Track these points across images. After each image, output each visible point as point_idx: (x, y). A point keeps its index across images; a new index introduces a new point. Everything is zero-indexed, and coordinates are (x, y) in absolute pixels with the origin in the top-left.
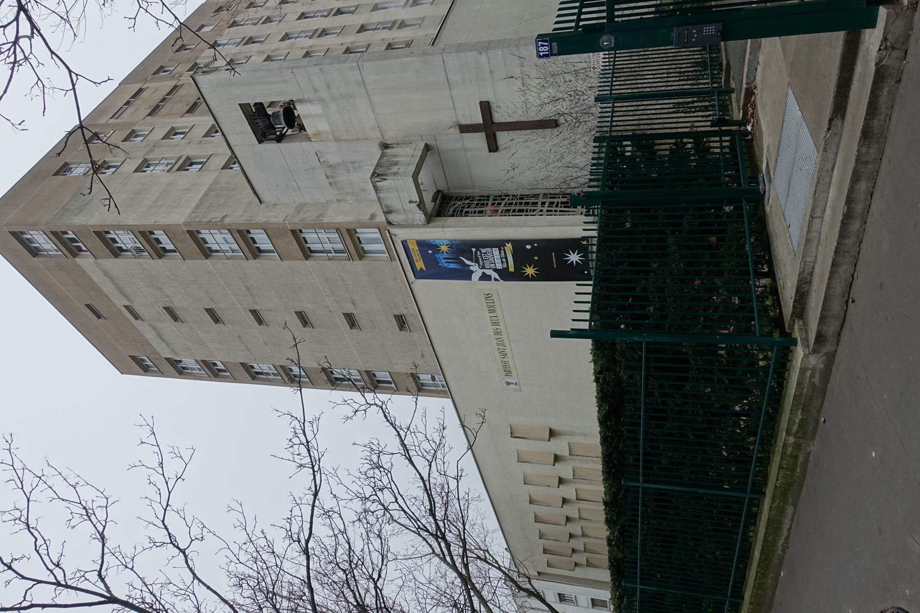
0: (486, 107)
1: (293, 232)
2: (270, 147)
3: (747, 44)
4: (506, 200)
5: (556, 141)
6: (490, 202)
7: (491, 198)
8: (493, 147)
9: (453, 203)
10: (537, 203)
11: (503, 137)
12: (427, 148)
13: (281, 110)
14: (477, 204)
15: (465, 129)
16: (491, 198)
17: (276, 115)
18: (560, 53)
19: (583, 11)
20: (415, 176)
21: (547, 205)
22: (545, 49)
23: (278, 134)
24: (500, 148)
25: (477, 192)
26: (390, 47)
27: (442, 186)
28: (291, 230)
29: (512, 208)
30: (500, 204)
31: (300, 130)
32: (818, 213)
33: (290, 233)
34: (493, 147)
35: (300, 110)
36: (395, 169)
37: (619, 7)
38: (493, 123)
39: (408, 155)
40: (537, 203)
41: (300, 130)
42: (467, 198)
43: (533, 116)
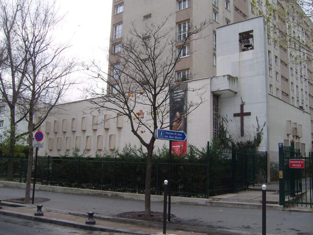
0: (249, 114)
1: (189, 19)
2: (237, 38)
3: (268, 206)
4: (217, 118)
5: (237, 136)
6: (216, 113)
7: (217, 113)
8: (236, 115)
9: (216, 99)
10: (216, 128)
11: (238, 118)
12: (236, 93)
13: (250, 44)
14: (216, 108)
15: (242, 106)
16: (217, 113)
17: (249, 42)
18: (279, 148)
19: (128, 113)
20: (229, 90)
21: (215, 132)
22: (280, 145)
23: (242, 40)
24: (235, 118)
25: (219, 108)
26: (271, 86)
27: (222, 96)
28: (190, 19)
29: (215, 120)
30: (216, 116)
31: (242, 50)
32: (240, 201)
33: (189, 18)
34: (236, 115)
35: (250, 52)
36: (231, 82)
37: (168, 216)
38: (243, 116)
39: (234, 88)
40: (216, 128)
41: (242, 50)
42: (217, 104)
43: (245, 129)
